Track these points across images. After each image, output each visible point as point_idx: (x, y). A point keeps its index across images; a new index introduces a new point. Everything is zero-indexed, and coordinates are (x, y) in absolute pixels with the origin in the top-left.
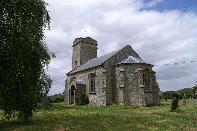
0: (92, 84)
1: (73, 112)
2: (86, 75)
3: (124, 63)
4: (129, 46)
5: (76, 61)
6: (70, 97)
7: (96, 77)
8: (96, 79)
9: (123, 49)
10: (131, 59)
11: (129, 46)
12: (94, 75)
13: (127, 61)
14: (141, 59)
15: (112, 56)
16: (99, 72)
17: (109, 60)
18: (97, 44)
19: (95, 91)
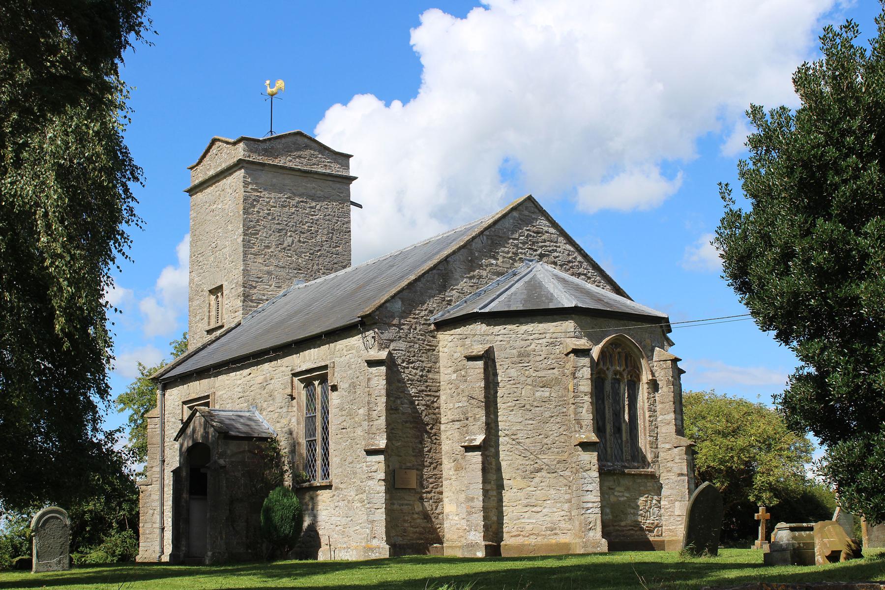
0: (317, 424)
1: (634, 468)
2: (278, 372)
3: (486, 310)
4: (530, 199)
5: (217, 291)
6: (319, 450)
7: (334, 388)
8: (334, 398)
9: (495, 223)
10: (534, 287)
11: (530, 199)
12: (323, 379)
13: (509, 299)
14: (618, 290)
15: (477, 231)
16: (349, 356)
17: (405, 293)
18: (352, 173)
19: (326, 475)
